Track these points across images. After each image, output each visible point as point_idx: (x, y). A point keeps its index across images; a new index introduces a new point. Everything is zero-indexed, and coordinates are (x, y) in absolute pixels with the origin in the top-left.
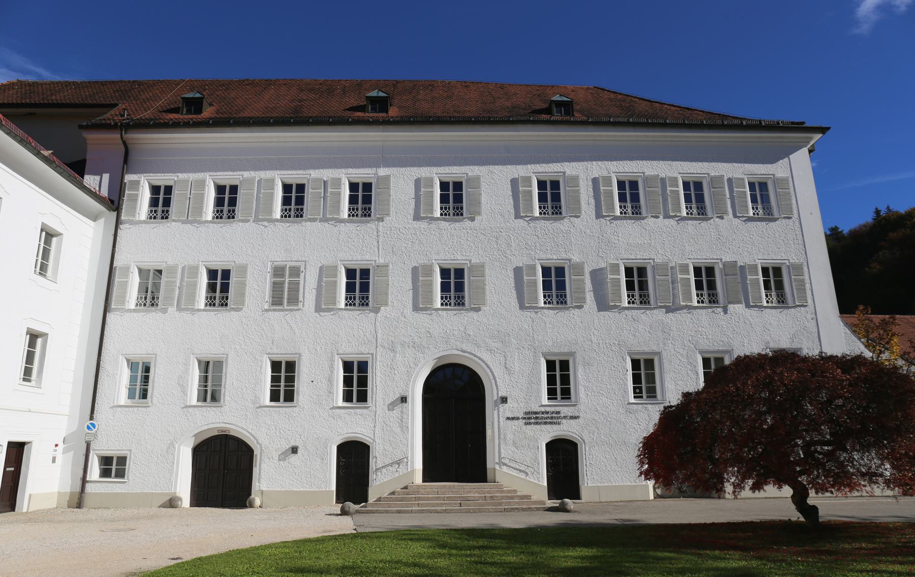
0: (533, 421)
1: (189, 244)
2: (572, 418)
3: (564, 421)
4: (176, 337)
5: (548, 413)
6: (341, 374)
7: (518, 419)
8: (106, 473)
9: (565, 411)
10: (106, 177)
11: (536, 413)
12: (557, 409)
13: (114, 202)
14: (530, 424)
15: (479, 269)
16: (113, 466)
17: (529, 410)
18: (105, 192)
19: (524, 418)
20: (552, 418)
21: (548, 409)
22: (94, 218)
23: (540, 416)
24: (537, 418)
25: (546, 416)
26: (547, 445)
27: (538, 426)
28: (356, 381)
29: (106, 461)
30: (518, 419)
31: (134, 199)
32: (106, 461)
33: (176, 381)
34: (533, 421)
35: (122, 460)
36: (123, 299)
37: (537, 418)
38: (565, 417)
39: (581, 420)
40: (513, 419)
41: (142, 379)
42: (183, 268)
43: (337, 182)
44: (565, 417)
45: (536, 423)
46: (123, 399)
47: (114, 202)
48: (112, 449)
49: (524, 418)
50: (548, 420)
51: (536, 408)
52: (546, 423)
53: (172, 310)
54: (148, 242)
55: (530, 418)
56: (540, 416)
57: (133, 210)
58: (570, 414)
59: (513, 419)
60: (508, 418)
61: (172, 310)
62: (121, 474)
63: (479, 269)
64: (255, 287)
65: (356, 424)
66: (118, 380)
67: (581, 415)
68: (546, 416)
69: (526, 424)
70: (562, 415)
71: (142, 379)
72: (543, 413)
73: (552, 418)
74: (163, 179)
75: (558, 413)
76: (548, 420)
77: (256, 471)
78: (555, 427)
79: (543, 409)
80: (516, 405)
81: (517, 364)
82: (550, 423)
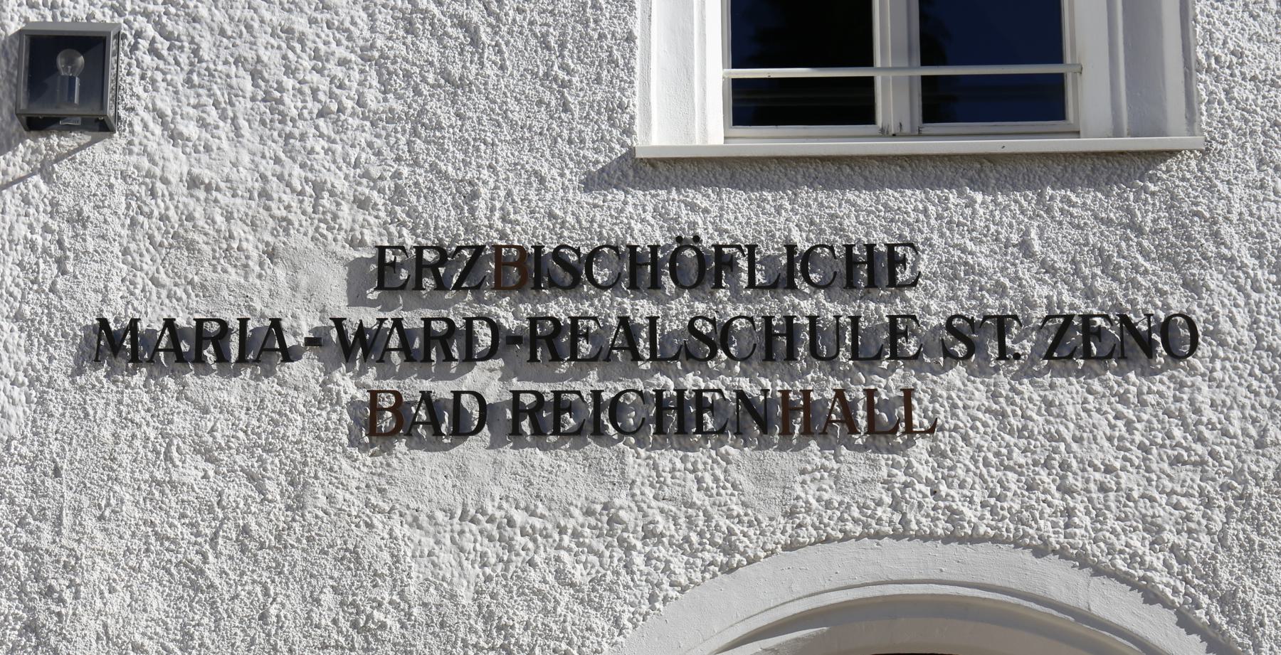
0: (487, 381)
2: (1078, 343)
3: (954, 390)
5: (710, 268)
7: (266, 347)
9: (976, 236)
11: (534, 270)
12: (860, 217)
14: (447, 423)
17: (444, 223)
19: (356, 346)
20: (776, 344)
21: (722, 217)
23: (602, 308)
24: (548, 342)
25: (679, 310)
27: (561, 470)
30: (266, 347)
34: (487, 381)
37: (548, 342)
38: (972, 339)
39: (1211, 386)
40: (196, 346)
42: (791, 355)
44: (972, 339)
45: (539, 421)
49: (356, 346)
50: (726, 381)
51: (539, 203)
52: (678, 420)
55: (441, 346)
56: (602, 308)
58: (1046, 295)
59: (196, 346)
60: (114, 345)
67: (1220, 303)
68: (679, 310)
69: (382, 425)
70: (932, 305)
72: (641, 270)
73: (776, 344)
75: (875, 268)
76: (726, 381)
78: (812, 475)
79: (642, 220)
80: (239, 157)
81: (591, 382)
82: (756, 420)
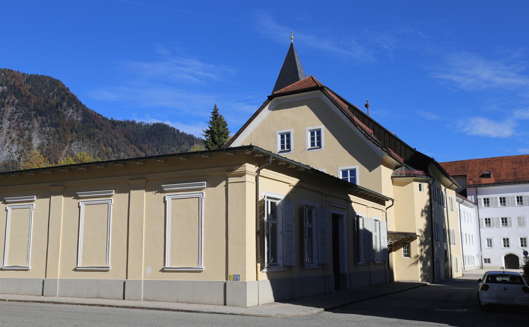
1: (495, 212)
4: (497, 233)
6: (503, 241)
8: (486, 262)
10: (473, 197)
13: (476, 203)
15: (510, 218)
16: (488, 261)
18: (474, 201)
22: (472, 207)
26: (505, 257)
28: (506, 242)
29: (485, 260)
31: (481, 203)
32: (485, 260)
33: (498, 243)
35: (489, 260)
36: (483, 225)
41: (490, 242)
43: (496, 198)
46: (487, 247)
47: (476, 203)
48: (487, 258)
53: (495, 227)
54: (486, 212)
57: (481, 205)
61: (495, 227)
62: (489, 262)
63: (510, 218)
64: (514, 221)
65: (508, 251)
66: (485, 243)
71: (490, 242)
74: (486, 196)
77: (410, 281)
